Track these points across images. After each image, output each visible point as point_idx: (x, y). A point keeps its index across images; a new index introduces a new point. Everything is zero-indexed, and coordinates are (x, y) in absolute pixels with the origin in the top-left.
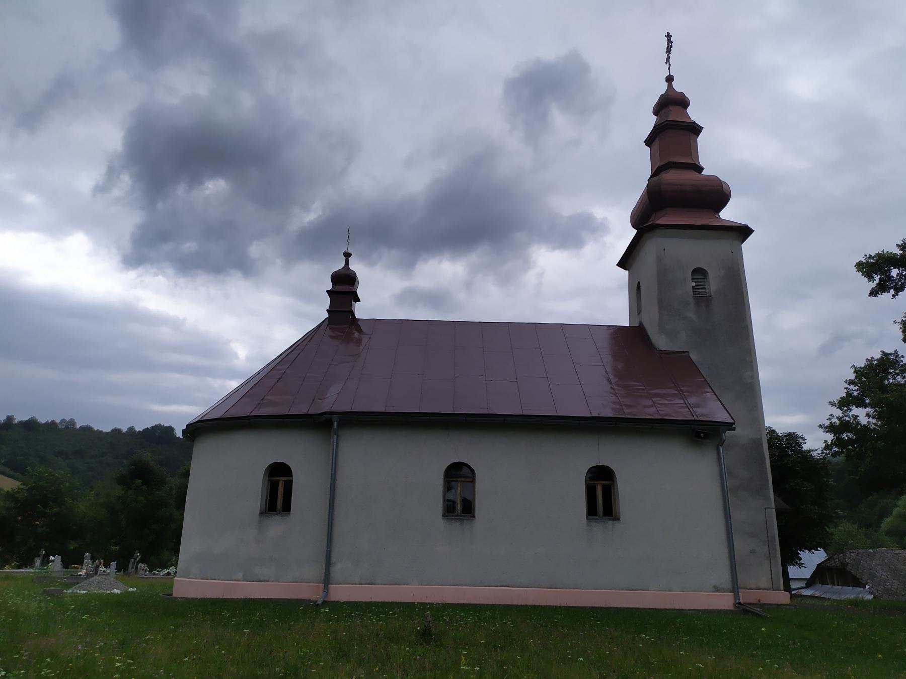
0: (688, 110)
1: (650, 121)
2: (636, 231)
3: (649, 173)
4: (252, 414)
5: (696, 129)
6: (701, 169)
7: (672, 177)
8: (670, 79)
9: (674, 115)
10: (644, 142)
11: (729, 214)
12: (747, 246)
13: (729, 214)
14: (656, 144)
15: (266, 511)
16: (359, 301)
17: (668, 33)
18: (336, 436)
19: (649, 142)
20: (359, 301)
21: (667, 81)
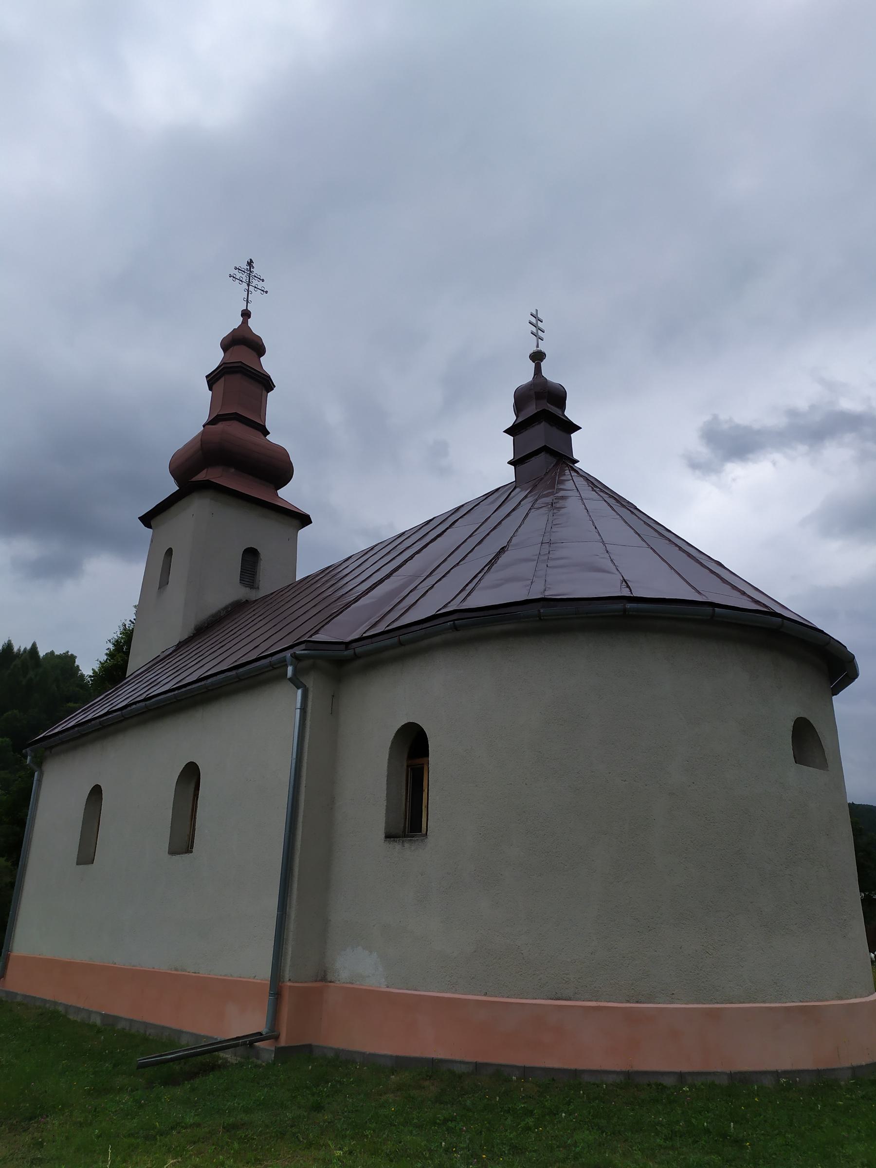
0: (262, 359)
1: (215, 357)
2: (178, 488)
3: (205, 418)
4: (480, 599)
5: (267, 384)
6: (267, 433)
7: (237, 431)
8: (246, 314)
9: (243, 355)
10: (207, 377)
11: (287, 494)
12: (304, 534)
13: (287, 494)
14: (220, 385)
15: (404, 831)
16: (577, 428)
17: (251, 261)
18: (300, 692)
19: (212, 380)
20: (577, 428)
21: (242, 315)
